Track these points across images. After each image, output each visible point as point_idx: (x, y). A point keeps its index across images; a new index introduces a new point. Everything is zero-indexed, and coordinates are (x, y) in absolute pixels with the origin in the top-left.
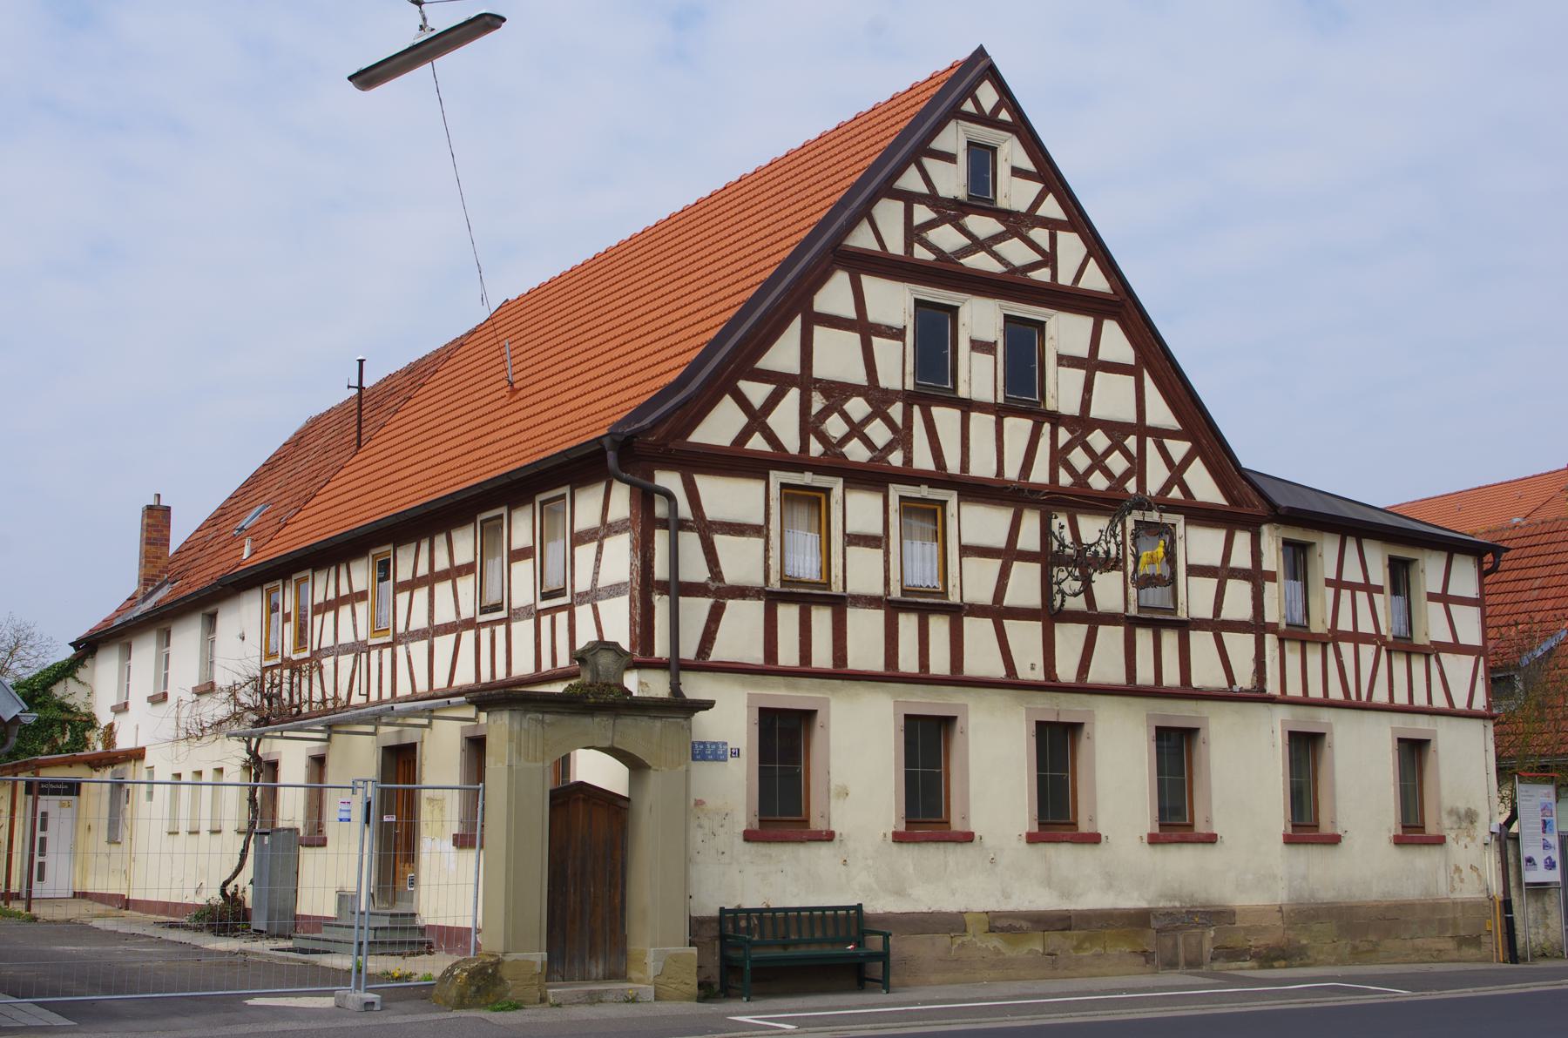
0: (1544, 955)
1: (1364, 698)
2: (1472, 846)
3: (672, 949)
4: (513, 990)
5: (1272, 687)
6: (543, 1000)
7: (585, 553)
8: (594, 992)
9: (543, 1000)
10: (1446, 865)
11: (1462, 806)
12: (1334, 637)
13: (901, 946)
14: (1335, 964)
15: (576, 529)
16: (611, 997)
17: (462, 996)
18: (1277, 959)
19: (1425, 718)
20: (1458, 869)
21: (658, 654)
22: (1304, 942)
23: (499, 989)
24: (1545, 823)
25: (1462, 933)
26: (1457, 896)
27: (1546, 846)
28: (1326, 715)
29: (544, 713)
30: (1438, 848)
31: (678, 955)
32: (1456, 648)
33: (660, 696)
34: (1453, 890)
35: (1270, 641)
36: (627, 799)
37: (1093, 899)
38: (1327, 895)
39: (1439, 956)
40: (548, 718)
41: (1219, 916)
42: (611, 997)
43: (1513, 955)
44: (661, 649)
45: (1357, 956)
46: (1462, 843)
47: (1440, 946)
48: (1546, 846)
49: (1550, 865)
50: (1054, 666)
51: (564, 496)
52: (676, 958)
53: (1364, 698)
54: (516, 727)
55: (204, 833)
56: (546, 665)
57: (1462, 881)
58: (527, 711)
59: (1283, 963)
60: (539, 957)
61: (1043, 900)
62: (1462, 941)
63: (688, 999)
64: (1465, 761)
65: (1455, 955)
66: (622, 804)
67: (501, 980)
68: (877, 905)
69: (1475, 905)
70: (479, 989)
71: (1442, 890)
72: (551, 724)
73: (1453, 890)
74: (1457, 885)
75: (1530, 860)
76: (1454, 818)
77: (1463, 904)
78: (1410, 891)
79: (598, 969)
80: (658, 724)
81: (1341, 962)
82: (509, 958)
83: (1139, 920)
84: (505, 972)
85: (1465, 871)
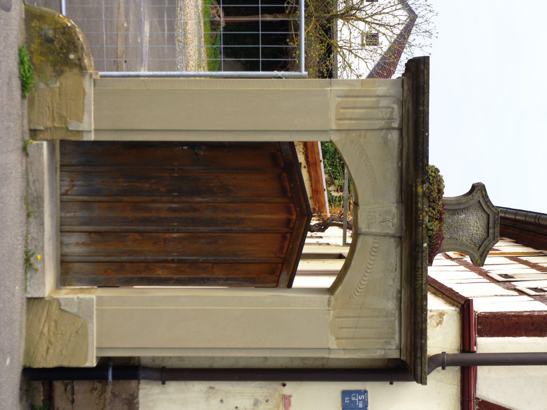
0: (21, 325)
3: (94, 328)
4: (48, 88)
6: (34, 133)
8: (40, 206)
9: (34, 133)
16: (34, 230)
17: (41, 17)
21: (481, 341)
23: (49, 69)
29: (400, 129)
31: (85, 336)
33: (428, 349)
36: (289, 285)
40: (394, 136)
42: (34, 230)
44: (486, 345)
50: (442, 286)
52: (82, 333)
54: (384, 102)
58: (402, 104)
60: (89, 127)
63: (27, 353)
66: (284, 277)
67: (59, 73)
70: (50, 41)
72: (385, 142)
79: (76, 246)
80: (391, 305)
82: (88, 86)
84: (70, 77)
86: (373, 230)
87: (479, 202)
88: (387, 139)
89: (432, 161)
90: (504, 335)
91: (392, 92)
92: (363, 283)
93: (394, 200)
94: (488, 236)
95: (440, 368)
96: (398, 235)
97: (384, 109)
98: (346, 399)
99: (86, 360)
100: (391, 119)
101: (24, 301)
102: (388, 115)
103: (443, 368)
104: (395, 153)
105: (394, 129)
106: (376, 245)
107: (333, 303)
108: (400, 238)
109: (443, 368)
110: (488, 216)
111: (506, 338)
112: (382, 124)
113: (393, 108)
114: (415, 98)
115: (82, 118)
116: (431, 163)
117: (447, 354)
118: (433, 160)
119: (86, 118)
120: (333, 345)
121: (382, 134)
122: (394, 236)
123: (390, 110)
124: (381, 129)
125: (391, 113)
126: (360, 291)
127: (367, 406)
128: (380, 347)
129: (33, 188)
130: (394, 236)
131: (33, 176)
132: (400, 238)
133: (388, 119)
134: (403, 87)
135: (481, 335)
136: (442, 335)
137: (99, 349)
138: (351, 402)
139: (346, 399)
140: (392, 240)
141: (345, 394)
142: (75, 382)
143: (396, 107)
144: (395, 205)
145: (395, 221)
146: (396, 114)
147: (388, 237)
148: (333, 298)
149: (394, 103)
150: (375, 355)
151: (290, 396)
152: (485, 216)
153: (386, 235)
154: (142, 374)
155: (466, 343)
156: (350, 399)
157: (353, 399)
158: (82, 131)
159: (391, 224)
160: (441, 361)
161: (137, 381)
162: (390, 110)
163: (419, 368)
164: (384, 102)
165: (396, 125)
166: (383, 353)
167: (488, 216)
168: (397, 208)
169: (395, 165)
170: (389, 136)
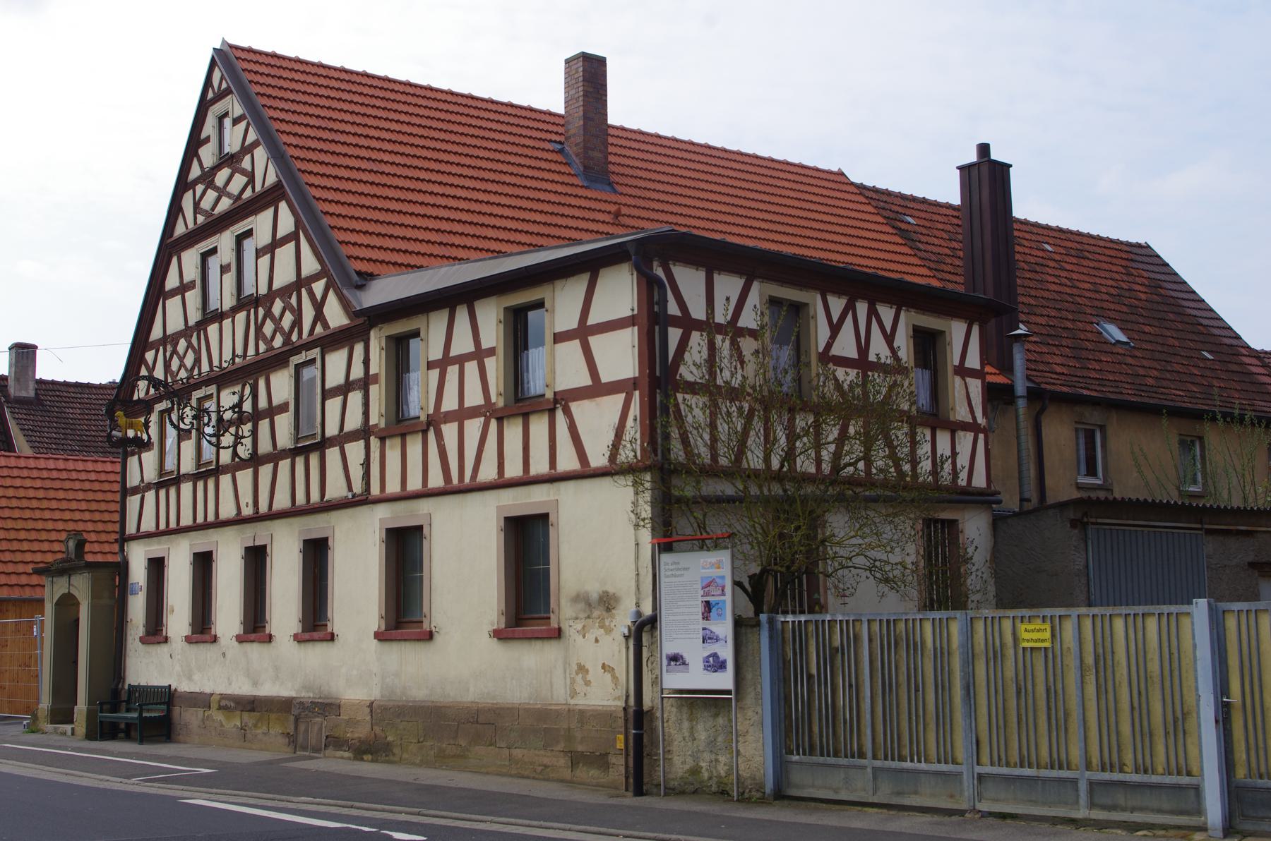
0: (723, 793)
1: (455, 481)
2: (606, 640)
5: (375, 490)
7: (334, 405)
10: (566, 663)
11: (594, 589)
12: (434, 422)
13: (188, 717)
14: (420, 765)
15: (327, 387)
18: (365, 752)
19: (545, 487)
20: (582, 669)
22: (390, 739)
24: (708, 606)
25: (580, 748)
26: (580, 702)
27: (708, 638)
28: (424, 506)
30: (554, 643)
32: (597, 389)
34: (574, 694)
35: (375, 443)
37: (269, 689)
38: (419, 694)
39: (543, 774)
41: (327, 707)
43: (639, 783)
45: (441, 760)
46: (591, 636)
47: (546, 761)
48: (708, 638)
49: (716, 665)
51: (313, 361)
53: (455, 481)
55: (865, 619)
56: (300, 499)
57: (587, 683)
59: (370, 757)
61: (243, 688)
62: (576, 759)
64: (601, 535)
65: (567, 774)
68: (184, 686)
69: (603, 716)
71: (558, 693)
73: (574, 694)
74: (580, 686)
75: (675, 658)
76: (582, 605)
77: (582, 712)
78: (516, 693)
81: (425, 763)
83: (282, 706)
85: (583, 671)
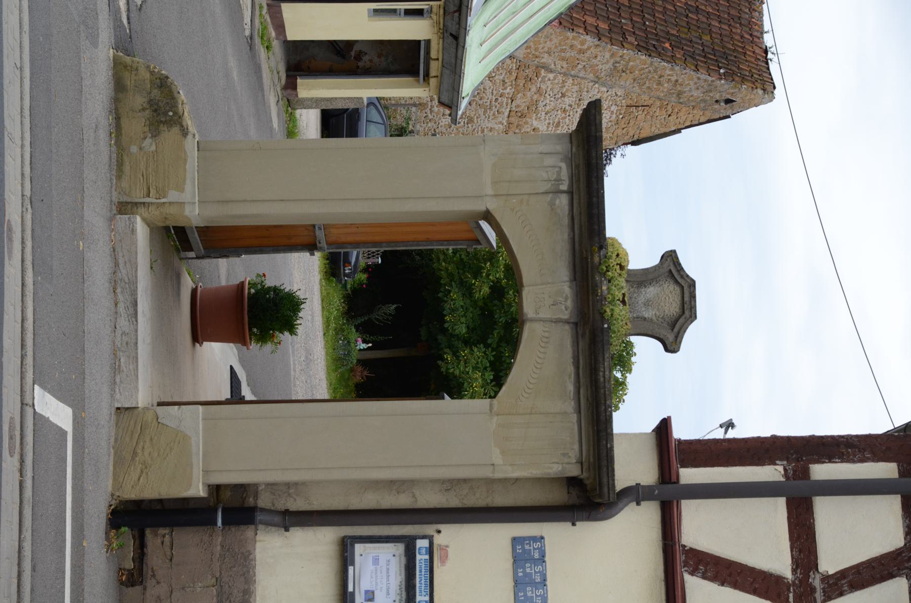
6: (125, 208)
29: (570, 193)
40: (563, 201)
44: (689, 475)
54: (549, 161)
72: (552, 204)
80: (569, 406)
84: (170, 135)
86: (541, 315)
87: (670, 271)
88: (555, 205)
89: (610, 232)
90: (713, 466)
91: (559, 148)
92: (532, 381)
93: (566, 279)
94: (683, 313)
95: (635, 503)
96: (572, 320)
97: (549, 169)
98: (520, 594)
99: (189, 486)
100: (558, 180)
101: (113, 410)
102: (555, 176)
103: (638, 504)
104: (566, 221)
105: (563, 192)
106: (546, 334)
107: (495, 409)
108: (576, 324)
109: (638, 504)
110: (682, 288)
111: (716, 468)
112: (547, 186)
113: (560, 168)
114: (595, 199)
115: (184, 189)
116: (608, 235)
117: (643, 486)
118: (611, 230)
119: (188, 187)
120: (497, 459)
121: (549, 199)
122: (567, 322)
123: (557, 169)
124: (547, 193)
125: (559, 173)
126: (529, 391)
127: (544, 556)
128: (556, 460)
129: (124, 271)
130: (567, 322)
131: (123, 256)
132: (576, 324)
133: (555, 180)
134: (571, 143)
135: (684, 466)
136: (633, 467)
137: (206, 472)
138: (526, 574)
139: (520, 594)
140: (567, 327)
141: (515, 541)
142: (175, 528)
143: (563, 165)
144: (568, 284)
145: (569, 303)
146: (565, 174)
147: (561, 324)
148: (495, 401)
149: (562, 160)
150: (550, 471)
151: (447, 546)
152: (678, 289)
153: (558, 321)
154: (259, 517)
155: (666, 475)
156: (523, 548)
157: (527, 547)
158: (184, 203)
159: (563, 307)
160: (636, 494)
161: (253, 527)
162: (557, 169)
163: (605, 469)
164: (549, 161)
165: (564, 187)
166: (560, 468)
167: (682, 288)
168: (570, 287)
169: (566, 236)
170: (557, 202)
